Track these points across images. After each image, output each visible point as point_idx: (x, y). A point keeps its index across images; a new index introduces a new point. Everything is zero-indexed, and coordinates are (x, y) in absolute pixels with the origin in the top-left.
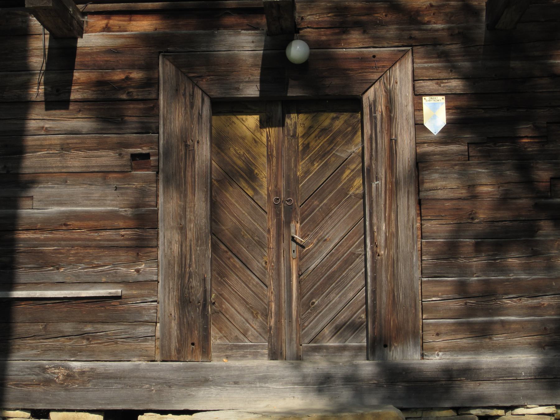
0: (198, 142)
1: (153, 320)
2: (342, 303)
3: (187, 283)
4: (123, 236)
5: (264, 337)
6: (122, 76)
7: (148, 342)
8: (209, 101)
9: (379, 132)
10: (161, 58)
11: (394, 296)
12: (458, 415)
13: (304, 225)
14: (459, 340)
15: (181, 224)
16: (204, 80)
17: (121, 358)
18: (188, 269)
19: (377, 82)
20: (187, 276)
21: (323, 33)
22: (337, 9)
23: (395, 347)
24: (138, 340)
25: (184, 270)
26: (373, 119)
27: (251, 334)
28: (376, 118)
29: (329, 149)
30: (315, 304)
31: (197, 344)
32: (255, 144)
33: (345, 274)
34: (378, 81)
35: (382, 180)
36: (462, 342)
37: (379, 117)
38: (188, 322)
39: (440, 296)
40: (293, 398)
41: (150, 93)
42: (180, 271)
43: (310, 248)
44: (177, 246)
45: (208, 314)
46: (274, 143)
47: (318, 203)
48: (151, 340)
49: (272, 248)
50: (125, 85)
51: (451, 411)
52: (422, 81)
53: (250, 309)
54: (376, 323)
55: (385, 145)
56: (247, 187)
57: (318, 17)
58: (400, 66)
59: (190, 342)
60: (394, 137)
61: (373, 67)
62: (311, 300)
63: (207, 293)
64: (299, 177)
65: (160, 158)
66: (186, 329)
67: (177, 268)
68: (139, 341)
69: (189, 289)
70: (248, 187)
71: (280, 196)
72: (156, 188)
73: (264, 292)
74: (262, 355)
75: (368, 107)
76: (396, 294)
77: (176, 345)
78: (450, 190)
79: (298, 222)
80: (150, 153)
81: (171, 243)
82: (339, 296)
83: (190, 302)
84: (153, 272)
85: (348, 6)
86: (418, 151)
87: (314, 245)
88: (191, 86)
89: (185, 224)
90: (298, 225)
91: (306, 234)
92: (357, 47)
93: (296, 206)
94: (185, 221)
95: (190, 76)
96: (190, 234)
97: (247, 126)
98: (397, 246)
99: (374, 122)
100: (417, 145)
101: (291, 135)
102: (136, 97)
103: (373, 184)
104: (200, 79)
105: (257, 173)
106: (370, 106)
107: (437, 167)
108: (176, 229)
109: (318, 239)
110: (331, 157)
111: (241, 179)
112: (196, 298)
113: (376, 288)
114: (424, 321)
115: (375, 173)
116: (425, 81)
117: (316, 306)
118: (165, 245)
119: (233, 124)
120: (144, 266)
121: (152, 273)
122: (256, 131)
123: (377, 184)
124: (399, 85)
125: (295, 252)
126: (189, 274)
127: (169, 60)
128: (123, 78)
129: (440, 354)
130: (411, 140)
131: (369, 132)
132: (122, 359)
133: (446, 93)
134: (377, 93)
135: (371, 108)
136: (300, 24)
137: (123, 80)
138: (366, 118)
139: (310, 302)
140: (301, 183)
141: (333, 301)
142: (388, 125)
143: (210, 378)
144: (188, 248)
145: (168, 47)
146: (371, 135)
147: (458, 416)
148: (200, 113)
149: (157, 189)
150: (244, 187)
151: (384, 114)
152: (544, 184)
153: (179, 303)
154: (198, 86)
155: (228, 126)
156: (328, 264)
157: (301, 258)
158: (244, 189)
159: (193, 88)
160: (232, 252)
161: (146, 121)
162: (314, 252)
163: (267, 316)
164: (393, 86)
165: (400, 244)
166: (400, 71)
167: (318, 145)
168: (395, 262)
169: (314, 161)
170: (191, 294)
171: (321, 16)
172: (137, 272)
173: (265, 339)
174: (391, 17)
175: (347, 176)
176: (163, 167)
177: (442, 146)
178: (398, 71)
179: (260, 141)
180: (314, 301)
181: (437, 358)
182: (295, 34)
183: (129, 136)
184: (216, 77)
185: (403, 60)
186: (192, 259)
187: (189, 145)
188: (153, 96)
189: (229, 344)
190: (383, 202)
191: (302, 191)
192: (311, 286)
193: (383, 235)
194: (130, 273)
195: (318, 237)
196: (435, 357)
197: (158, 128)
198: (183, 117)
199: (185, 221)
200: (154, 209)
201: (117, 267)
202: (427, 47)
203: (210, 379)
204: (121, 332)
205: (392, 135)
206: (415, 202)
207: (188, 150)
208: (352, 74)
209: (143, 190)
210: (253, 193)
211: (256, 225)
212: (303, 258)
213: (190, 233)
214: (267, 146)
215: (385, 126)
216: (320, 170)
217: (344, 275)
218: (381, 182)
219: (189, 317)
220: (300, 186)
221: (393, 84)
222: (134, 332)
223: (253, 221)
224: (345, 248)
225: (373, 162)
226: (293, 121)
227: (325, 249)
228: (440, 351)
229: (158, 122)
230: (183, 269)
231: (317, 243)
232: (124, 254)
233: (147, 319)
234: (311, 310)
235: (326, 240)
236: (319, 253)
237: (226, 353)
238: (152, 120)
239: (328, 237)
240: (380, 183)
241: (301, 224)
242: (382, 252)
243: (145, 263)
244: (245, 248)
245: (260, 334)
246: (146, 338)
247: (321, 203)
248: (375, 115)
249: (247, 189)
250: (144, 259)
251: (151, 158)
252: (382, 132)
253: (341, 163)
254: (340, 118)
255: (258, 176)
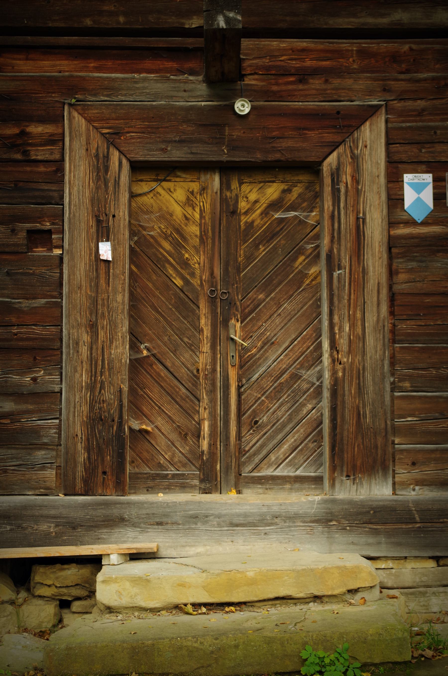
0: (114, 216)
1: (53, 442)
2: (293, 423)
3: (98, 396)
4: (16, 335)
5: (194, 465)
6: (16, 131)
7: (46, 471)
8: (129, 165)
9: (343, 208)
10: (66, 107)
11: (359, 414)
12: (439, 566)
13: (245, 324)
14: (440, 471)
15: (90, 321)
16: (122, 138)
17: (12, 491)
18: (99, 378)
19: (341, 146)
20: (99, 386)
21: (273, 81)
22: (293, 51)
23: (360, 479)
24: (35, 467)
25: (95, 379)
26: (336, 192)
27: (178, 460)
28: (339, 190)
29: (278, 229)
30: (259, 423)
31: (109, 474)
32: (186, 221)
33: (297, 386)
34: (343, 144)
35: (345, 268)
36: (444, 473)
37: (343, 190)
38: (98, 444)
39: (417, 415)
40: (231, 543)
41: (51, 154)
42: (89, 381)
43: (253, 353)
44: (86, 348)
45: (124, 435)
46: (209, 221)
47: (264, 297)
48: (50, 468)
49: (206, 353)
50: (20, 142)
51: (431, 561)
52: (398, 145)
53: (177, 429)
54: (337, 449)
55: (349, 222)
56: (174, 275)
57: (267, 61)
58: (371, 125)
59: (100, 470)
60: (361, 215)
61: (336, 126)
62: (253, 419)
63: (123, 408)
64: (240, 264)
65: (64, 236)
66: (95, 454)
67: (85, 376)
68: (35, 469)
69: (100, 403)
70: (177, 275)
71: (216, 287)
72: (58, 274)
73: (195, 407)
74: (193, 487)
75: (330, 177)
76: (362, 413)
77: (82, 474)
78: (431, 282)
79: (238, 321)
80: (53, 230)
81: (77, 344)
82: (288, 413)
83: (102, 420)
84: (54, 381)
85: (307, 47)
86: (392, 233)
87: (259, 349)
88: (106, 146)
89: (97, 320)
90: (238, 325)
91: (248, 335)
92: (316, 100)
93: (236, 300)
94: (97, 316)
95: (103, 132)
96: (102, 334)
97: (175, 198)
98: (364, 352)
99: (337, 195)
100: (390, 225)
101: (231, 211)
102: (33, 158)
103: (334, 273)
104: (117, 137)
105: (187, 258)
106: (332, 175)
107: (415, 254)
108: (86, 327)
109: (263, 342)
110: (280, 239)
111: (167, 265)
112: (108, 415)
113: (336, 404)
114: (396, 446)
115: (336, 260)
116: (402, 145)
117: (260, 425)
118: (70, 347)
119: (158, 195)
120: (43, 373)
121: (53, 382)
122: (187, 204)
123: (339, 274)
124: (369, 150)
125: (234, 358)
126: (101, 385)
127: (77, 110)
128: (18, 132)
129: (417, 488)
130: (382, 220)
131: (331, 208)
132: (13, 493)
133: (427, 160)
134: (342, 159)
135: (334, 178)
136: (245, 69)
137: (17, 135)
138: (328, 189)
139: (252, 421)
140: (243, 271)
141: (281, 421)
142: (354, 201)
143: (126, 516)
144: (100, 352)
145: (77, 95)
146: (333, 212)
147: (440, 568)
148: (117, 179)
149: (60, 276)
150: (171, 275)
151: (349, 186)
152: (336, 356)
153: (88, 421)
154: (115, 146)
155: (152, 197)
156: (275, 373)
157: (241, 367)
158: (171, 278)
159: (108, 149)
160: (155, 357)
161: (46, 188)
162: (259, 358)
163: (199, 436)
164: (361, 150)
165: (368, 349)
166: (371, 131)
167: (264, 225)
168: (361, 372)
169: (259, 244)
170: (103, 409)
171: (272, 60)
172: (33, 381)
173: (196, 467)
174: (361, 63)
175: (301, 264)
176: (69, 248)
177: (422, 227)
178: (368, 131)
179: (192, 218)
180: (257, 419)
181: (413, 493)
182: (239, 82)
183: (24, 207)
184: (138, 134)
185: (374, 118)
186: (105, 365)
187: (103, 221)
188: (57, 156)
189: (149, 473)
190: (346, 297)
191: (244, 282)
192: (254, 401)
193: (346, 337)
194: (24, 382)
195: (263, 339)
196: (410, 492)
197: (62, 197)
198: (94, 184)
199: (97, 316)
200: (57, 301)
201: (7, 374)
202: (405, 102)
203: (126, 518)
204: (8, 458)
205: (360, 213)
206: (387, 298)
207: (100, 226)
208: (310, 135)
209: (43, 277)
210: (182, 284)
211: (186, 323)
212: (245, 365)
213: (102, 332)
214: (200, 225)
215: (351, 201)
216: (267, 255)
217: (295, 388)
218: (345, 271)
219: (100, 439)
220: (242, 275)
221: (361, 148)
222: (28, 457)
223: (182, 318)
224: (297, 354)
225: (335, 246)
226: (234, 194)
227: (272, 355)
228: (417, 485)
229: (63, 191)
230: (93, 378)
231: (262, 347)
232: (16, 358)
233: (45, 441)
234: (254, 431)
235: (273, 343)
236: (264, 360)
237: (147, 484)
238: (54, 187)
239: (277, 339)
240: (343, 273)
241: (242, 323)
242: (345, 360)
243: (44, 370)
244: (172, 352)
245: (189, 460)
246: (44, 466)
247: (267, 297)
248: (338, 187)
249: (175, 278)
250: (43, 364)
251: (53, 236)
252: (346, 207)
253: (294, 246)
254: (293, 190)
255: (189, 262)
